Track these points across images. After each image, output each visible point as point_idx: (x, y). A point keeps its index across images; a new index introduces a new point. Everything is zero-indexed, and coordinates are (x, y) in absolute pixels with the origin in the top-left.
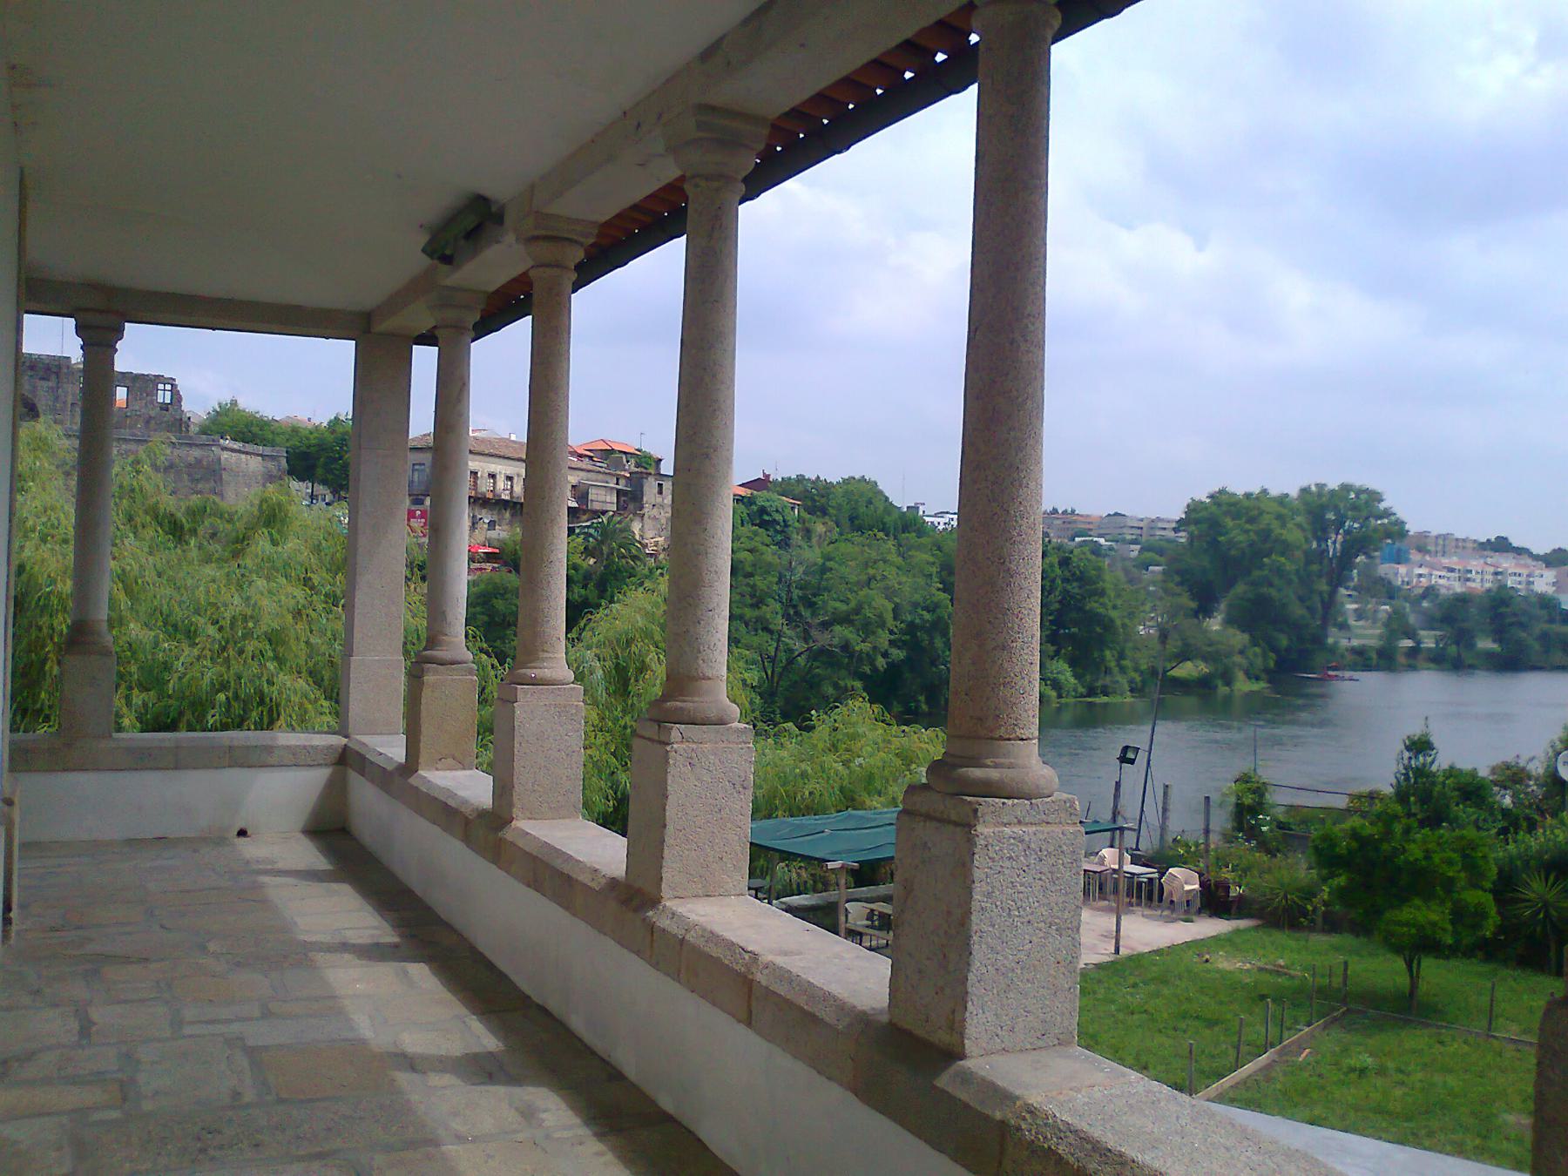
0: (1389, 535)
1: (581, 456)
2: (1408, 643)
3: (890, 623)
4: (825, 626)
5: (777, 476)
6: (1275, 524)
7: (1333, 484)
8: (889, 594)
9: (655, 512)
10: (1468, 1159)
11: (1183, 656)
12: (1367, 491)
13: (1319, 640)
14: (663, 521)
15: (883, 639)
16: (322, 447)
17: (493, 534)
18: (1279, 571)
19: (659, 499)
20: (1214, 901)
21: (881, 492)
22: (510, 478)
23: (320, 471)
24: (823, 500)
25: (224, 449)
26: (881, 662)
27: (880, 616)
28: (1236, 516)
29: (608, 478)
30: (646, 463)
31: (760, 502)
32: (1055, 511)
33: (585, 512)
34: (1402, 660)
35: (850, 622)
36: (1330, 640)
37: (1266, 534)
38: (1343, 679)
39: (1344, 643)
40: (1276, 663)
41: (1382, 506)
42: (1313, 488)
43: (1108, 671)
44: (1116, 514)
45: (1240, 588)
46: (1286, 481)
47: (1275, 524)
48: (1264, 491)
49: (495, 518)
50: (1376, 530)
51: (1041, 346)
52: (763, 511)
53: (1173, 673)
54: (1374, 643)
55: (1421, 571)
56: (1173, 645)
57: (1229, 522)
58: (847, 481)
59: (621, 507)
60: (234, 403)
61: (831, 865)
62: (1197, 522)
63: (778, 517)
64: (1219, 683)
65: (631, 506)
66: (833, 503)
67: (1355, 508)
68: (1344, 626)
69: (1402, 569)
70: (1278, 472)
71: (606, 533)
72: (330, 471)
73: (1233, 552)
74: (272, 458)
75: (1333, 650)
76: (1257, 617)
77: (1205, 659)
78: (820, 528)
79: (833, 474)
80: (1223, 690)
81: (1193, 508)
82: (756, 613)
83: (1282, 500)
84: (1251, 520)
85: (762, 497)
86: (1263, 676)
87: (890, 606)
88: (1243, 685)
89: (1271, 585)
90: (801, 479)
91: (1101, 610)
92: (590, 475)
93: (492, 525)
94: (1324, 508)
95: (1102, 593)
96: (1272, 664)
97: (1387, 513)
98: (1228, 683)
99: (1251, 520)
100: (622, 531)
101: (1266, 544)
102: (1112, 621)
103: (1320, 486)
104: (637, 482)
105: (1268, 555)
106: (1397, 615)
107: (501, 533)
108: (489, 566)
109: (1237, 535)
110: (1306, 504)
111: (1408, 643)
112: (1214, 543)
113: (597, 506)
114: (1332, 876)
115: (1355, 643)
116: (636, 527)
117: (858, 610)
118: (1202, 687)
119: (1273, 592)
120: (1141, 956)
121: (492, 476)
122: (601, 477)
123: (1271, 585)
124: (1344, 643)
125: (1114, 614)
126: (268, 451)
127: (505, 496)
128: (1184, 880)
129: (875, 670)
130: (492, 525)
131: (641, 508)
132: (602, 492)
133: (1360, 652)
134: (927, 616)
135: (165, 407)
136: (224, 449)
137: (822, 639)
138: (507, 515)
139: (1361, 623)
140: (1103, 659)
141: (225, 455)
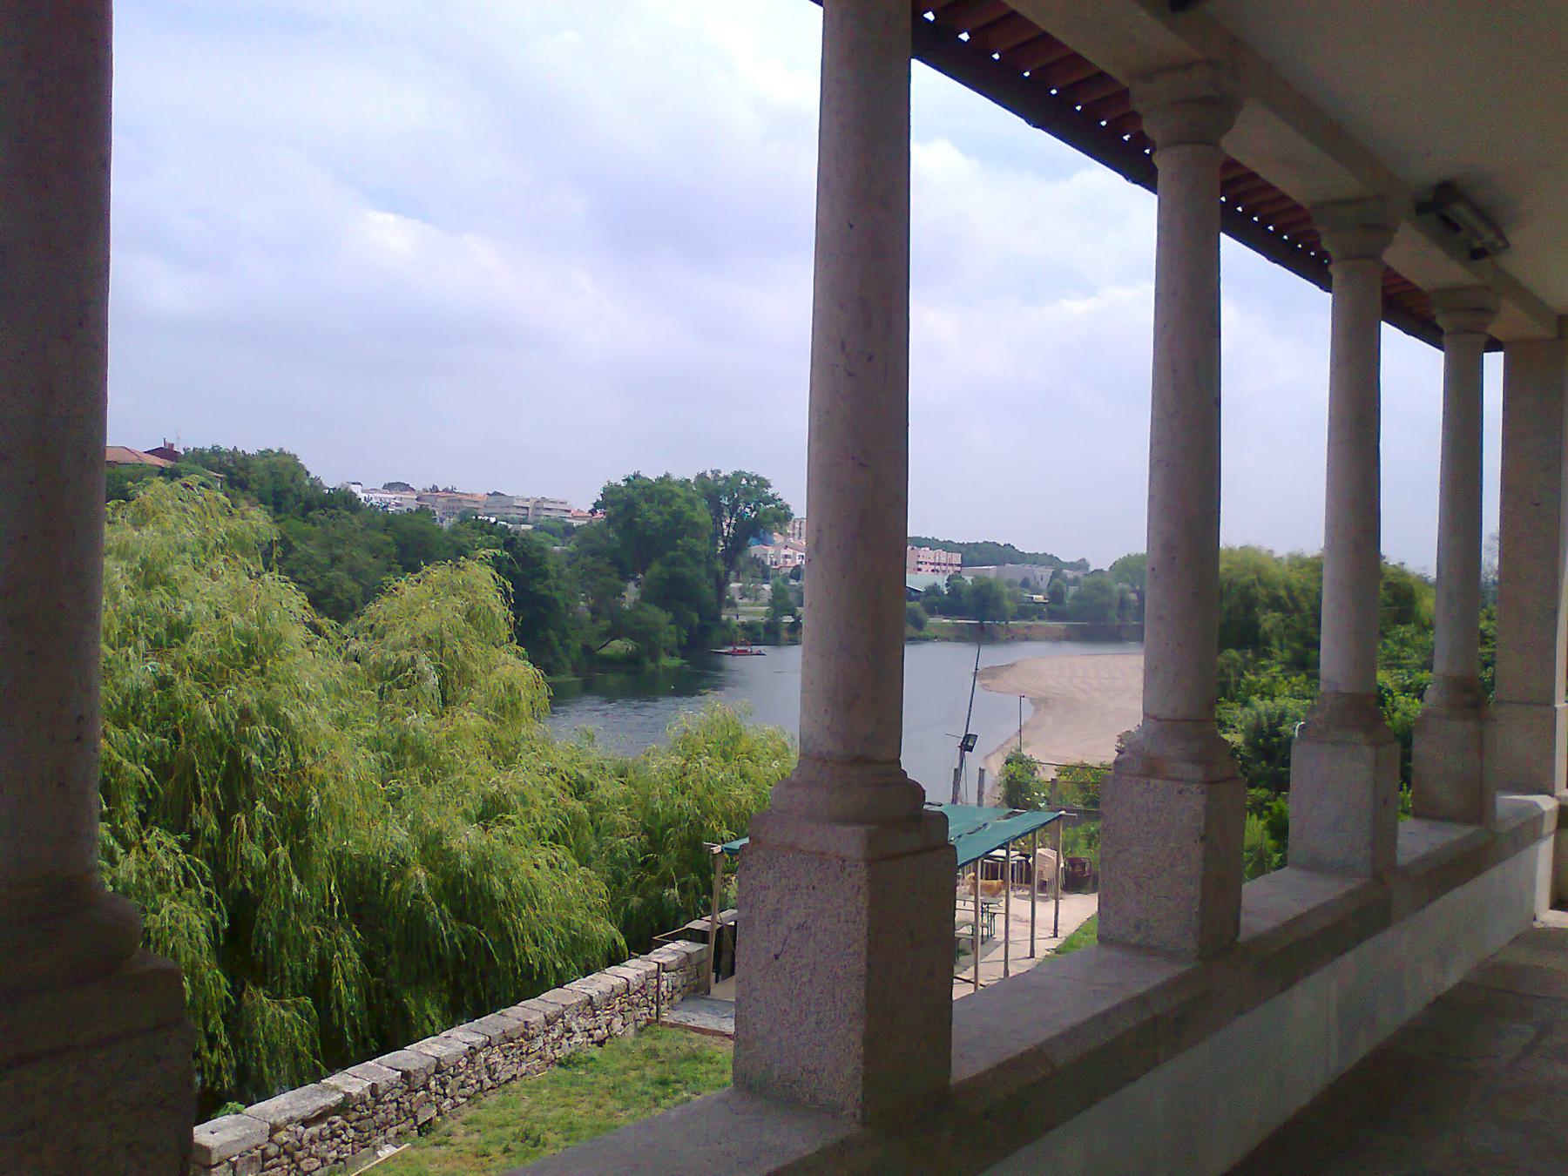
0: (777, 519)
2: (789, 619)
6: (687, 507)
7: (727, 471)
11: (613, 634)
12: (756, 477)
13: (716, 617)
18: (692, 553)
21: (301, 467)
24: (242, 474)
28: (649, 499)
30: (739, 508)
32: (435, 489)
34: (784, 634)
36: (724, 617)
37: (677, 516)
38: (751, 654)
39: (735, 621)
40: (689, 638)
41: (770, 492)
42: (709, 475)
43: (552, 652)
44: (496, 494)
45: (656, 568)
46: (684, 470)
47: (687, 507)
48: (667, 476)
50: (765, 513)
51: (1151, 497)
53: (605, 651)
54: (762, 619)
55: (789, 552)
56: (605, 624)
57: (644, 506)
58: (265, 454)
62: (613, 504)
64: (647, 659)
67: (747, 492)
68: (732, 604)
69: (771, 550)
70: (678, 460)
73: (648, 532)
75: (726, 626)
76: (672, 593)
77: (633, 636)
80: (650, 666)
81: (610, 493)
83: (685, 483)
84: (665, 503)
86: (677, 652)
88: (670, 662)
89: (684, 565)
90: (216, 451)
91: (546, 592)
94: (719, 491)
95: (546, 575)
96: (684, 640)
97: (773, 499)
98: (654, 659)
99: (665, 503)
101: (678, 526)
102: (555, 600)
103: (716, 473)
105: (681, 537)
106: (778, 594)
109: (650, 514)
110: (705, 487)
111: (789, 619)
112: (630, 524)
115: (743, 619)
118: (631, 663)
119: (686, 572)
123: (684, 565)
124: (735, 621)
125: (557, 595)
133: (749, 628)
139: (745, 600)
140: (548, 639)
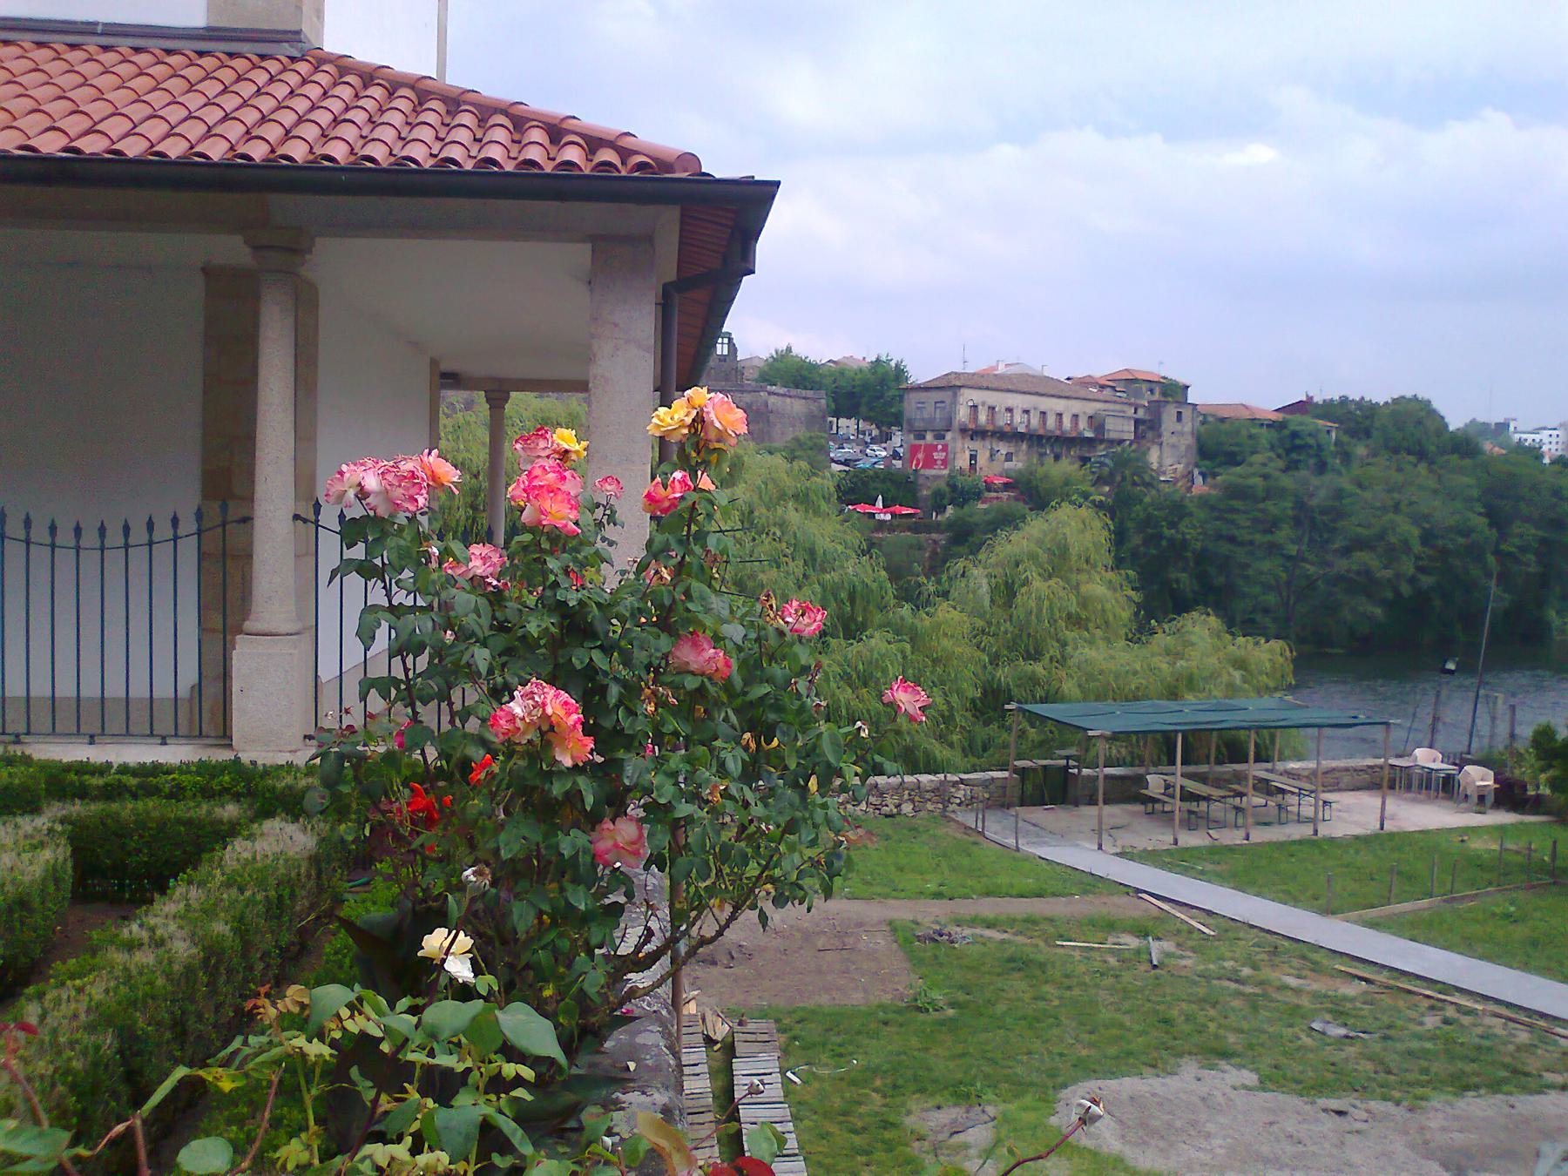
1: (1103, 387)
3: (1417, 547)
4: (1346, 551)
5: (1318, 399)
8: (1417, 519)
9: (1174, 439)
10: (1209, 881)
14: (1183, 448)
15: (1408, 568)
16: (865, 386)
17: (1008, 465)
19: (1178, 427)
20: (1509, 795)
22: (1027, 412)
23: (863, 409)
24: (1367, 423)
25: (770, 393)
26: (1405, 589)
27: (1406, 542)
29: (1125, 408)
31: (1292, 427)
33: (1102, 441)
35: (1372, 548)
49: (1012, 450)
52: (1295, 435)
59: (1139, 437)
60: (789, 349)
61: (1090, 733)
63: (1311, 441)
65: (1150, 435)
66: (1377, 424)
71: (1121, 462)
72: (871, 409)
74: (815, 400)
78: (1361, 450)
79: (1380, 394)
82: (1269, 537)
85: (1295, 420)
87: (1416, 532)
90: (1344, 401)
92: (1106, 406)
93: (1009, 457)
100: (1137, 459)
104: (1156, 409)
107: (1017, 464)
108: (1004, 495)
113: (1113, 436)
114: (1550, 766)
116: (1153, 457)
117: (1381, 536)
120: (1408, 835)
121: (1010, 410)
122: (1118, 407)
126: (810, 393)
127: (1022, 429)
128: (1479, 777)
129: (1398, 594)
130: (1009, 457)
131: (1160, 436)
132: (1120, 421)
134: (1461, 540)
135: (723, 358)
136: (770, 393)
137: (1342, 565)
138: (1024, 446)
141: (772, 399)
